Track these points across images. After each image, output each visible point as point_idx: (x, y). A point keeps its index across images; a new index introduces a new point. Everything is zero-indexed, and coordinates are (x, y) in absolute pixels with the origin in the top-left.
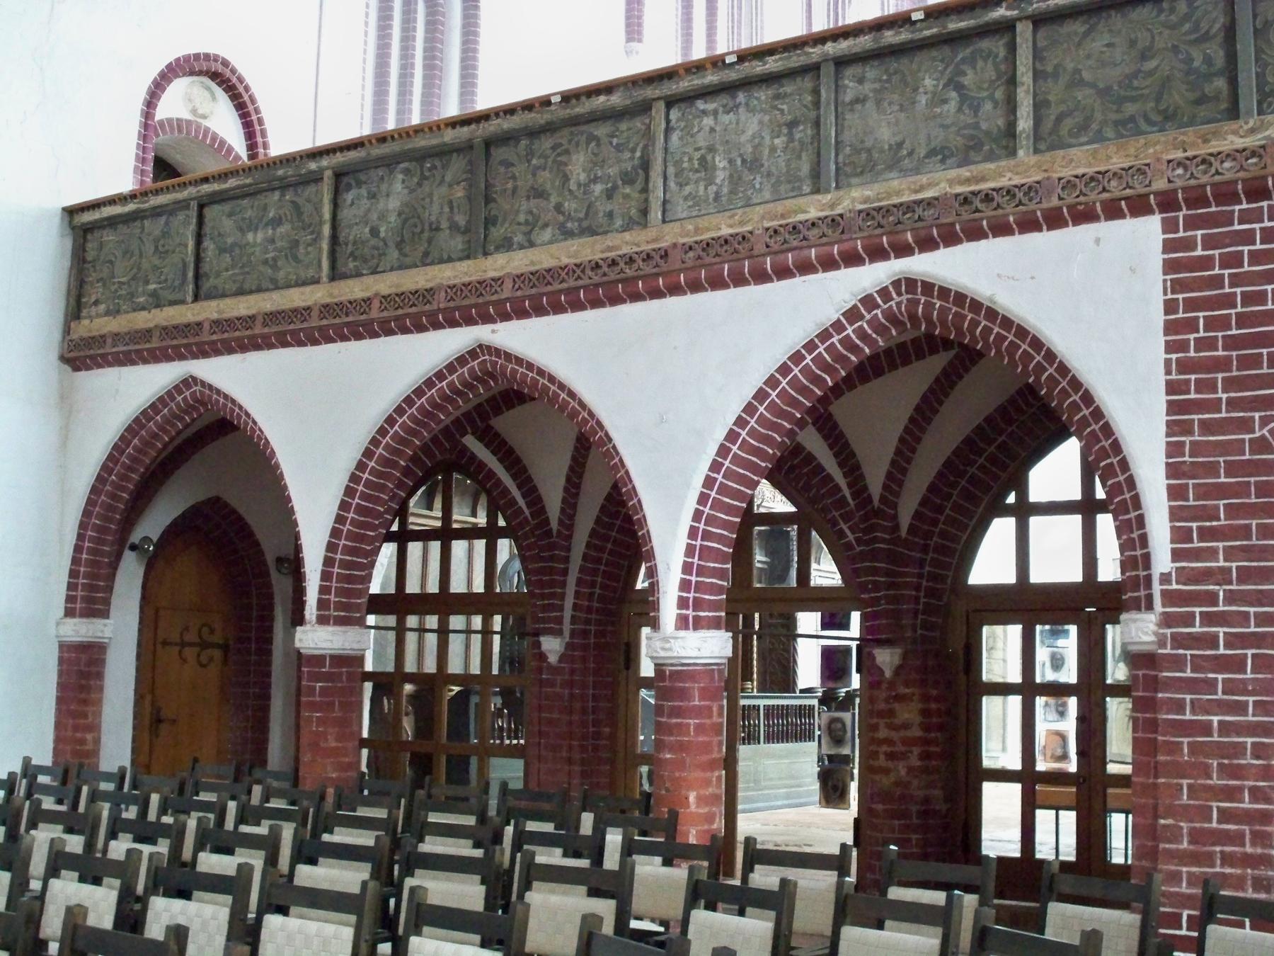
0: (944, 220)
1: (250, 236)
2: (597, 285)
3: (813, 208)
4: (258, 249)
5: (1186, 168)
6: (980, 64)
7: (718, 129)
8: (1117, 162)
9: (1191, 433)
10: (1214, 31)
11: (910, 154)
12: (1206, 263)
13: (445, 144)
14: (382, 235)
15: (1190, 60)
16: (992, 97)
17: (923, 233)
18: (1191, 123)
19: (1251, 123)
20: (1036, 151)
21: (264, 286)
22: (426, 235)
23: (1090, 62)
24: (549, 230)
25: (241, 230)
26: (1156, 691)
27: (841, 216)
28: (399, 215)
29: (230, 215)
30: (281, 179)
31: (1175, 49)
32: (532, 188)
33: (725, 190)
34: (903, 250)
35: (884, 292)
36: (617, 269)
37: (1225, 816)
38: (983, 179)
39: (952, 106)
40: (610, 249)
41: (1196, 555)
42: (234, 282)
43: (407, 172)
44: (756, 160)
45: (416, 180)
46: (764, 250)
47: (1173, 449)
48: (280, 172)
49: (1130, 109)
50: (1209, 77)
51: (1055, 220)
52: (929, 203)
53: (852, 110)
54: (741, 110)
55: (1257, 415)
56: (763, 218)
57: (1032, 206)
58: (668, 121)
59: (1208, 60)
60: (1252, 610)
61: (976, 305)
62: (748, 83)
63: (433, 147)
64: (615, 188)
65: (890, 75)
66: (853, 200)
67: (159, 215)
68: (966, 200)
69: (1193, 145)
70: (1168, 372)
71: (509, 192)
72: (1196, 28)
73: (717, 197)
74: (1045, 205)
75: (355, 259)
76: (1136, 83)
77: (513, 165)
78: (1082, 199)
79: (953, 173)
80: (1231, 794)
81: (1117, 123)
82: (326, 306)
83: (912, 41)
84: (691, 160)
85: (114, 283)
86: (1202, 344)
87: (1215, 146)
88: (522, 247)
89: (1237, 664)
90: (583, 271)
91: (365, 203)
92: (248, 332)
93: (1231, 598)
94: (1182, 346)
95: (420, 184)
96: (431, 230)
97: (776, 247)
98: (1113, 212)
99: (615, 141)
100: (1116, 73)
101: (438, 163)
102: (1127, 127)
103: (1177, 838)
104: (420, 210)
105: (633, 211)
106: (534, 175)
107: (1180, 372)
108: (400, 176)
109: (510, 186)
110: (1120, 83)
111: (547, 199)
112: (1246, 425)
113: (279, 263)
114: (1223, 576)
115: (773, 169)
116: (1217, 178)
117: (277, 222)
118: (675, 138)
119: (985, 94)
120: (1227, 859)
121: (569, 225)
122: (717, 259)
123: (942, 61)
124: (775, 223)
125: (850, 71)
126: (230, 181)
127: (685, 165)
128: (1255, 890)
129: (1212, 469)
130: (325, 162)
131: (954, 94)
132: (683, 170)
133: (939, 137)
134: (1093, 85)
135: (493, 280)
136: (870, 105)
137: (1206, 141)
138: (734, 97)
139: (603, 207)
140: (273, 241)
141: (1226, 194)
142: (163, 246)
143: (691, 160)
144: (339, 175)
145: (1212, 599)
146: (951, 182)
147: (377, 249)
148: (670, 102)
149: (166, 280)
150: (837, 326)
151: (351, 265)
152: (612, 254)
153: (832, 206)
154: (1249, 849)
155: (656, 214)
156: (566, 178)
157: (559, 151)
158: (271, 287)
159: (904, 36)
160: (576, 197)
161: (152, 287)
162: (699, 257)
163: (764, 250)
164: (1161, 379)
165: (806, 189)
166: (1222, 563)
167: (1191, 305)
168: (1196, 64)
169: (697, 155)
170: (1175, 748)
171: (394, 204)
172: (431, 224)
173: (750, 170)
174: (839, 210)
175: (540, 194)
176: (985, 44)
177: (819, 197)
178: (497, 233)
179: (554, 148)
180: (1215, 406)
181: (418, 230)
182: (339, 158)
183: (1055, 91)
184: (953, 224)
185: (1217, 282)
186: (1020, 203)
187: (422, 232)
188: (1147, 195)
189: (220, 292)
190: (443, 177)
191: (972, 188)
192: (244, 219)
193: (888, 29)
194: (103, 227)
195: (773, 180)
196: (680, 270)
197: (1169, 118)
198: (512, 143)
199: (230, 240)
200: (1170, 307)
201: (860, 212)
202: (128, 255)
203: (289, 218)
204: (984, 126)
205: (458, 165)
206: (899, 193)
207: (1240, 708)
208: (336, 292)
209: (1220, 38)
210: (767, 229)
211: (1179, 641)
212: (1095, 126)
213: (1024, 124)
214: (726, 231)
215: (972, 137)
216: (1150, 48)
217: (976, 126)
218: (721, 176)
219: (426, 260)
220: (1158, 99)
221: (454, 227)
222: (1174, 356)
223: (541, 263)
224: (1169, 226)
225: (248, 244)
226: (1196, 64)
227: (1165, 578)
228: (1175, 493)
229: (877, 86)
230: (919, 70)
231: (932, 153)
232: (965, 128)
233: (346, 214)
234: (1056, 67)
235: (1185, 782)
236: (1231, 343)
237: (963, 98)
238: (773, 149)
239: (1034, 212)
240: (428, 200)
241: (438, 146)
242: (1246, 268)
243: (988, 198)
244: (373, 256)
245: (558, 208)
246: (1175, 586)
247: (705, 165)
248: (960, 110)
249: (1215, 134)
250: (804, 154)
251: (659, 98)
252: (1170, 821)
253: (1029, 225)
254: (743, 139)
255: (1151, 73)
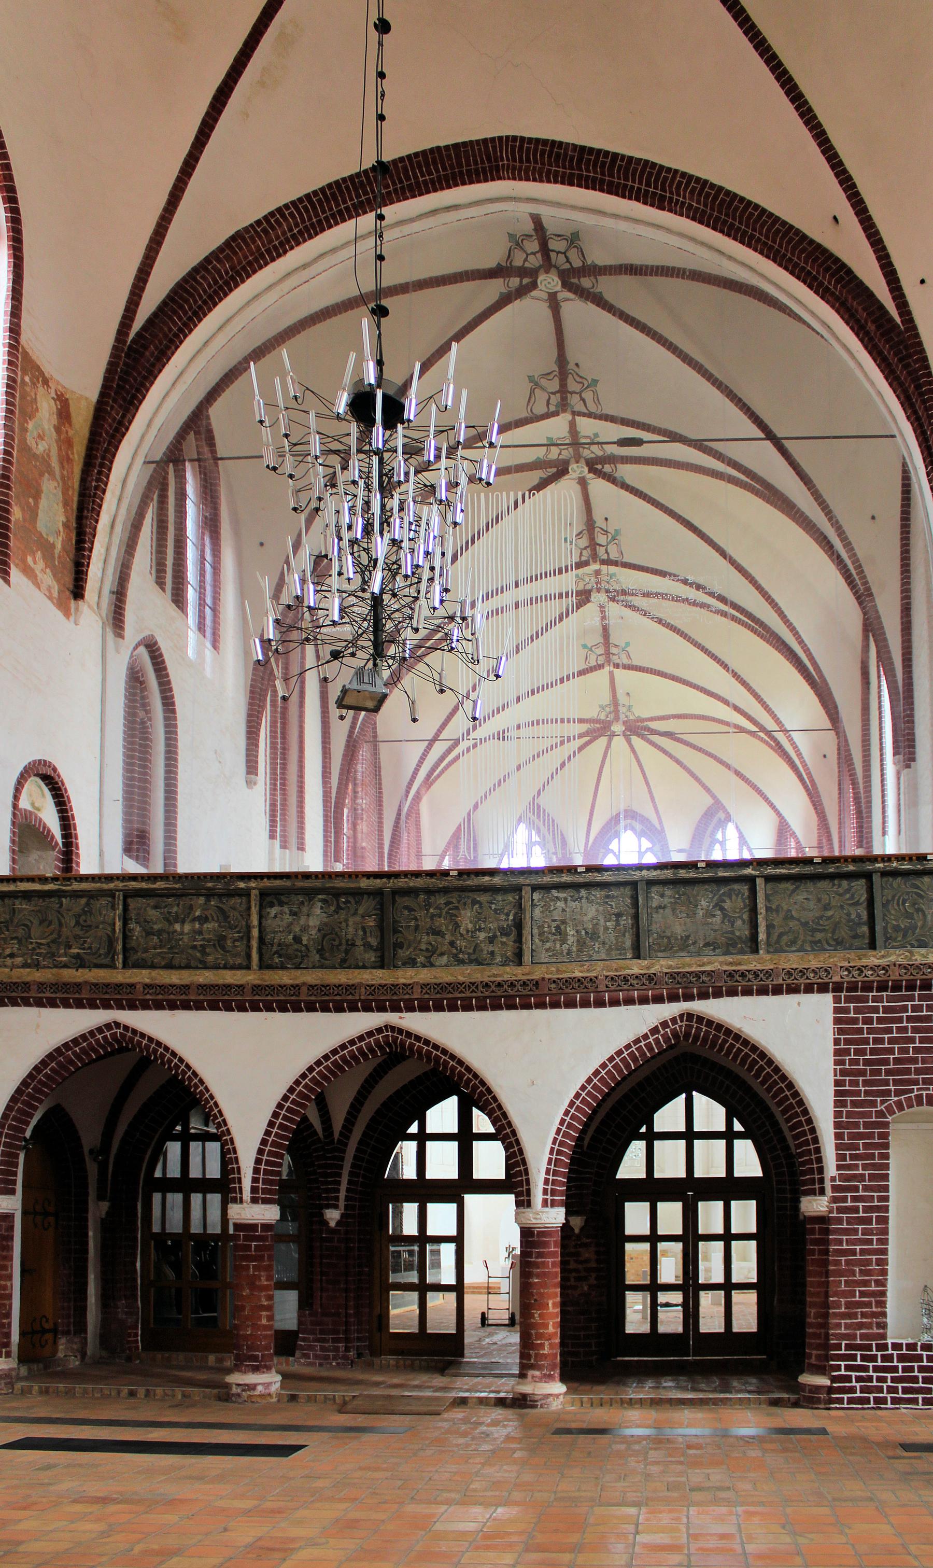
0: (717, 984)
1: (177, 927)
2: (486, 997)
3: (636, 968)
4: (186, 937)
5: (850, 972)
6: (734, 897)
7: (568, 910)
8: (814, 963)
9: (846, 1106)
10: (861, 901)
11: (694, 944)
12: (855, 1021)
13: (360, 888)
14: (305, 942)
15: (849, 914)
16: (741, 917)
17: (703, 990)
18: (850, 948)
19: (883, 953)
20: (768, 952)
21: (193, 965)
22: (343, 948)
23: (796, 907)
24: (445, 957)
25: (168, 920)
26: (828, 1235)
27: (655, 974)
28: (319, 930)
29: (156, 907)
30: (209, 889)
31: (842, 907)
32: (431, 928)
33: (574, 949)
34: (689, 997)
35: (674, 1020)
36: (502, 989)
37: (862, 1294)
38: (740, 964)
39: (718, 919)
40: (495, 976)
41: (849, 1167)
42: (163, 958)
43: (324, 901)
44: (594, 933)
45: (333, 908)
46: (605, 989)
47: (837, 1114)
48: (210, 885)
49: (819, 936)
50: (859, 924)
51: (777, 991)
52: (709, 974)
53: (657, 912)
54: (584, 901)
55: (879, 1099)
56: (603, 970)
57: (768, 982)
58: (533, 900)
59: (859, 916)
60: (875, 1194)
61: (728, 1032)
62: (588, 885)
63: (350, 888)
64: (495, 936)
65: (680, 895)
66: (662, 966)
67: (82, 897)
68: (731, 975)
69: (854, 960)
70: (835, 1075)
71: (413, 928)
72: (852, 897)
73: (569, 953)
74: (775, 983)
75: (280, 956)
76: (821, 922)
77: (415, 911)
78: (795, 981)
79: (722, 958)
80: (866, 1283)
81: (811, 942)
82: (258, 986)
83: (696, 878)
84: (549, 927)
85: (32, 943)
86: (852, 1062)
87: (864, 962)
88: (424, 966)
89: (868, 1221)
90: (477, 987)
91: (288, 918)
92: (183, 997)
93: (866, 1188)
94: (842, 1062)
95: (336, 912)
96: (347, 944)
97: (613, 988)
98: (809, 989)
99: (493, 906)
100: (811, 914)
101: (351, 899)
102: (817, 946)
103: (839, 1307)
104: (337, 929)
105: (509, 953)
106: (432, 919)
107: (841, 1076)
108: (319, 904)
109: (412, 923)
110: (813, 921)
111: (443, 937)
112: (873, 1104)
113: (208, 950)
114: (861, 1178)
115: (607, 941)
116: (866, 979)
117: (204, 919)
118: (537, 911)
119: (737, 915)
120: (864, 1315)
121: (461, 956)
122: (573, 991)
123: (711, 892)
124: (612, 974)
125: (654, 889)
126: (158, 883)
127: (546, 929)
128: (877, 1328)
129: (856, 1125)
130: (253, 884)
131: (719, 912)
132: (544, 932)
133: (711, 937)
134: (799, 920)
135: (404, 985)
136: (668, 911)
137: (860, 959)
138: (579, 892)
139: (486, 948)
140: (200, 932)
141: (867, 987)
142: (85, 921)
143: (549, 927)
144: (263, 894)
145: (856, 1189)
146: (721, 963)
147: (301, 951)
148: (535, 888)
149: (90, 948)
150: (645, 1037)
151: (277, 960)
152: (499, 979)
153: (648, 968)
154: (874, 1309)
155: (527, 958)
156: (457, 926)
157: (451, 906)
158: (200, 966)
159: (692, 874)
160: (465, 939)
161: (75, 951)
162: (561, 988)
163: (605, 989)
164: (831, 1079)
165: (629, 955)
166: (861, 1172)
167: (847, 1042)
168: (853, 917)
169: (554, 924)
170: (838, 1263)
171: (314, 922)
172: (347, 941)
173: (591, 938)
174: (652, 971)
175: (438, 933)
176: (736, 886)
177: (640, 961)
178: (403, 953)
179: (447, 904)
180: (858, 1093)
181: (336, 943)
182: (266, 883)
183: (777, 920)
184: (722, 987)
185: (860, 1031)
186: (761, 980)
187: (340, 944)
188: (828, 983)
189: (149, 964)
190: (357, 910)
191: (734, 968)
192: (169, 913)
193: (682, 869)
194: (16, 897)
195: (607, 947)
196: (547, 995)
197: (839, 944)
198: (413, 895)
199: (156, 927)
200: (836, 1042)
201: (666, 973)
202: (46, 923)
203: (216, 918)
204: (737, 934)
205: (367, 905)
206: (690, 965)
207: (870, 1242)
208: (266, 977)
209: (865, 904)
210: (607, 977)
211: (840, 1210)
212: (799, 943)
213: (762, 936)
214: (578, 974)
215: (731, 939)
216: (829, 904)
217: (732, 933)
218: (571, 940)
219: (344, 964)
220: (833, 933)
221: (368, 946)
222: (838, 1067)
223: (441, 978)
224: (837, 1000)
225: (176, 931)
226: (853, 917)
227: (833, 1179)
228: (838, 1136)
229: (672, 900)
230: (698, 895)
231: (707, 945)
232: (726, 933)
233: (269, 923)
234: (778, 906)
235: (843, 1279)
236: (867, 1062)
237: (725, 916)
238: (606, 928)
239: (768, 985)
240: (344, 924)
241: (355, 888)
242: (875, 1025)
243: (743, 975)
244: (296, 956)
245: (452, 944)
246: (838, 1183)
247: (560, 932)
248: (723, 922)
249: (865, 956)
250: (627, 934)
251: (528, 885)
252: (835, 1299)
253: (763, 991)
254: (585, 919)
255: (829, 918)
